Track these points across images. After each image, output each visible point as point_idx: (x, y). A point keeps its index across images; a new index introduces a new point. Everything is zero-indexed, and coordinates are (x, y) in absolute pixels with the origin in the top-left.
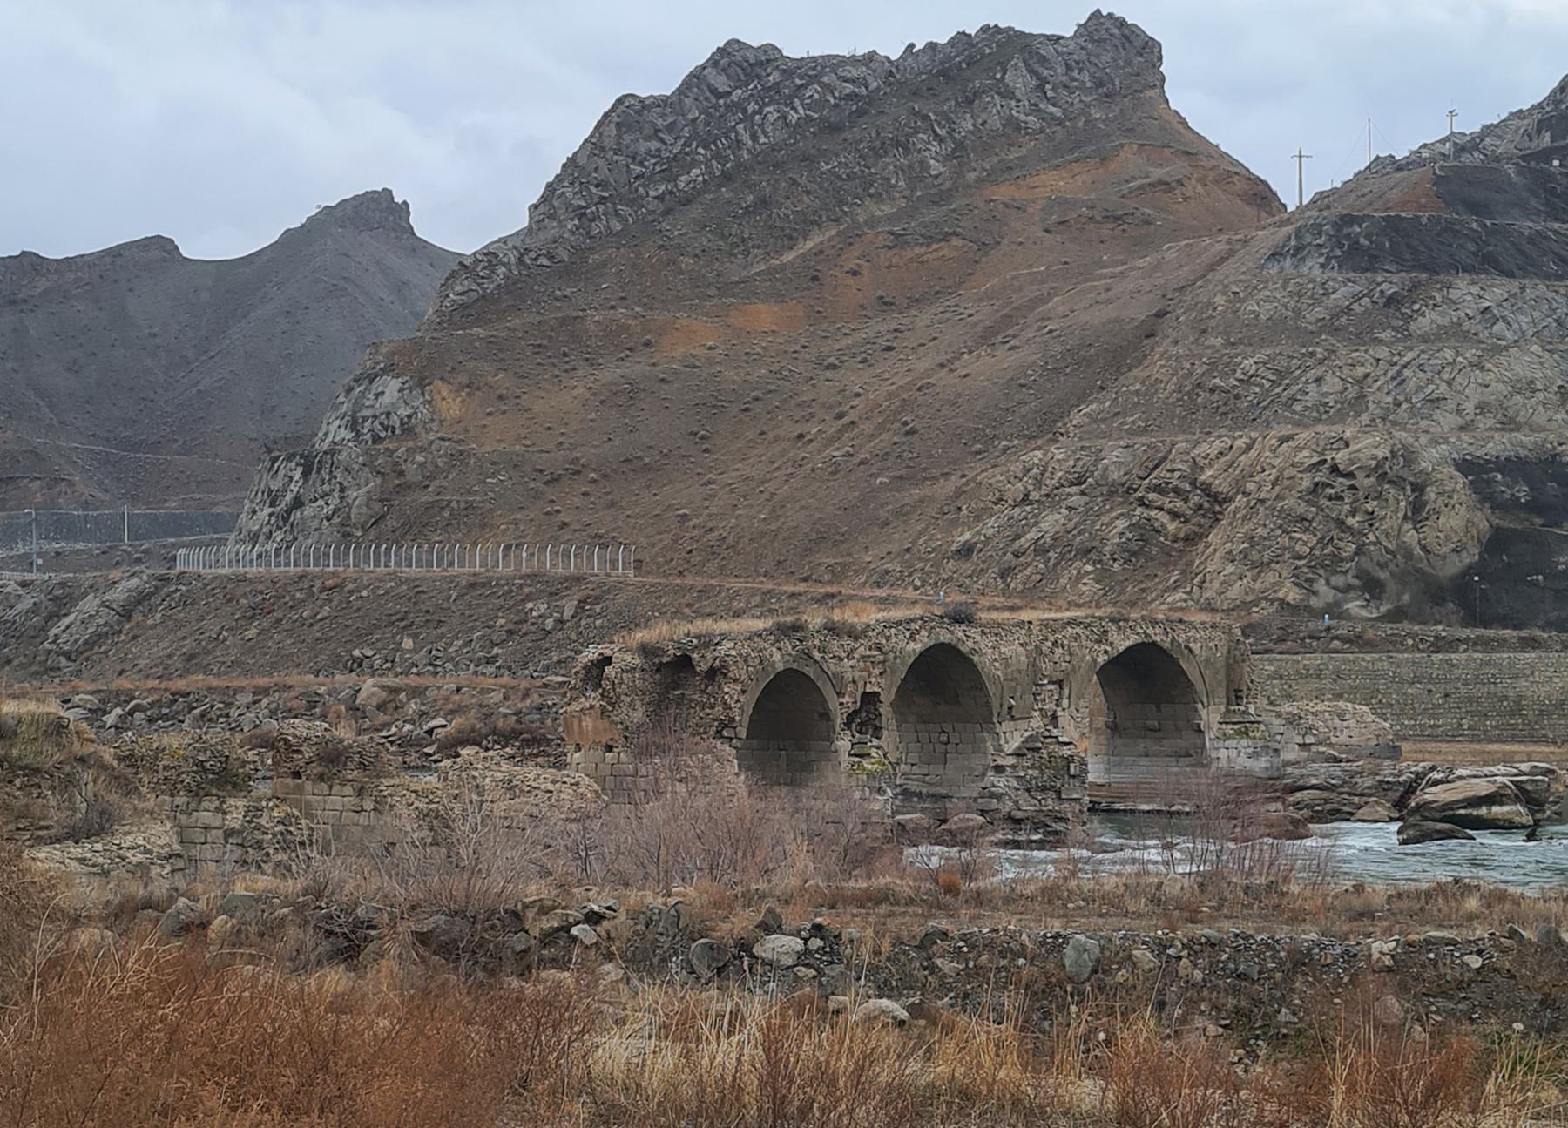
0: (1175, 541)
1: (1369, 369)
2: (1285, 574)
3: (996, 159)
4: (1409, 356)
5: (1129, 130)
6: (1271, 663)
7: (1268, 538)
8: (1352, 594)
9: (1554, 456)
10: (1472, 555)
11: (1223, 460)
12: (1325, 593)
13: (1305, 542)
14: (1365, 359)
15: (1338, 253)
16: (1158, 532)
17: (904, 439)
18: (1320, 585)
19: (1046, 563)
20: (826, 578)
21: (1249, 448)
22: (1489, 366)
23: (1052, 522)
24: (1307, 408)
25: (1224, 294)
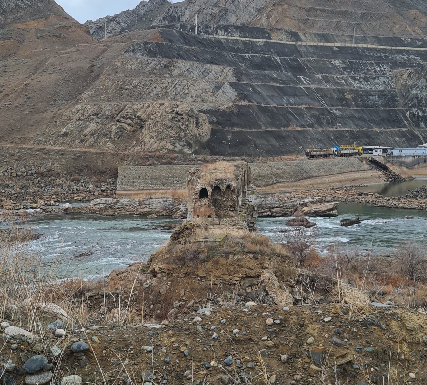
0: (130, 132)
1: (167, 85)
2: (168, 142)
3: (14, 16)
4: (176, 82)
5: (50, 10)
6: (185, 167)
7: (163, 132)
8: (185, 147)
9: (218, 109)
10: (209, 136)
11: (142, 110)
12: (179, 147)
13: (172, 133)
14: (166, 81)
15: (146, 52)
16: (125, 129)
17: (27, 100)
18: (177, 145)
19: (94, 138)
20: (19, 142)
21: (149, 106)
22: (196, 85)
23: (92, 127)
24: (154, 95)
25: (119, 62)
